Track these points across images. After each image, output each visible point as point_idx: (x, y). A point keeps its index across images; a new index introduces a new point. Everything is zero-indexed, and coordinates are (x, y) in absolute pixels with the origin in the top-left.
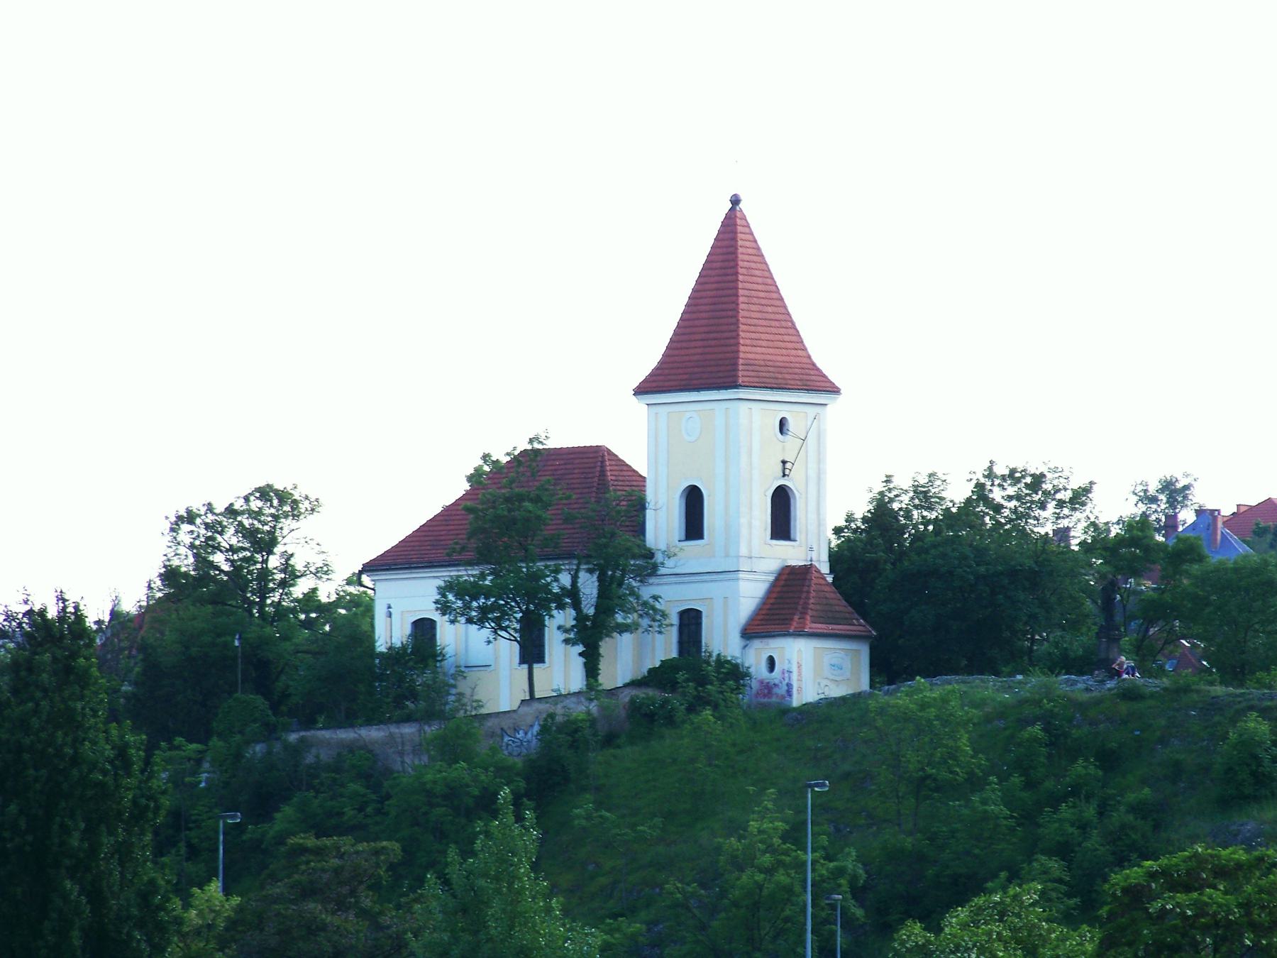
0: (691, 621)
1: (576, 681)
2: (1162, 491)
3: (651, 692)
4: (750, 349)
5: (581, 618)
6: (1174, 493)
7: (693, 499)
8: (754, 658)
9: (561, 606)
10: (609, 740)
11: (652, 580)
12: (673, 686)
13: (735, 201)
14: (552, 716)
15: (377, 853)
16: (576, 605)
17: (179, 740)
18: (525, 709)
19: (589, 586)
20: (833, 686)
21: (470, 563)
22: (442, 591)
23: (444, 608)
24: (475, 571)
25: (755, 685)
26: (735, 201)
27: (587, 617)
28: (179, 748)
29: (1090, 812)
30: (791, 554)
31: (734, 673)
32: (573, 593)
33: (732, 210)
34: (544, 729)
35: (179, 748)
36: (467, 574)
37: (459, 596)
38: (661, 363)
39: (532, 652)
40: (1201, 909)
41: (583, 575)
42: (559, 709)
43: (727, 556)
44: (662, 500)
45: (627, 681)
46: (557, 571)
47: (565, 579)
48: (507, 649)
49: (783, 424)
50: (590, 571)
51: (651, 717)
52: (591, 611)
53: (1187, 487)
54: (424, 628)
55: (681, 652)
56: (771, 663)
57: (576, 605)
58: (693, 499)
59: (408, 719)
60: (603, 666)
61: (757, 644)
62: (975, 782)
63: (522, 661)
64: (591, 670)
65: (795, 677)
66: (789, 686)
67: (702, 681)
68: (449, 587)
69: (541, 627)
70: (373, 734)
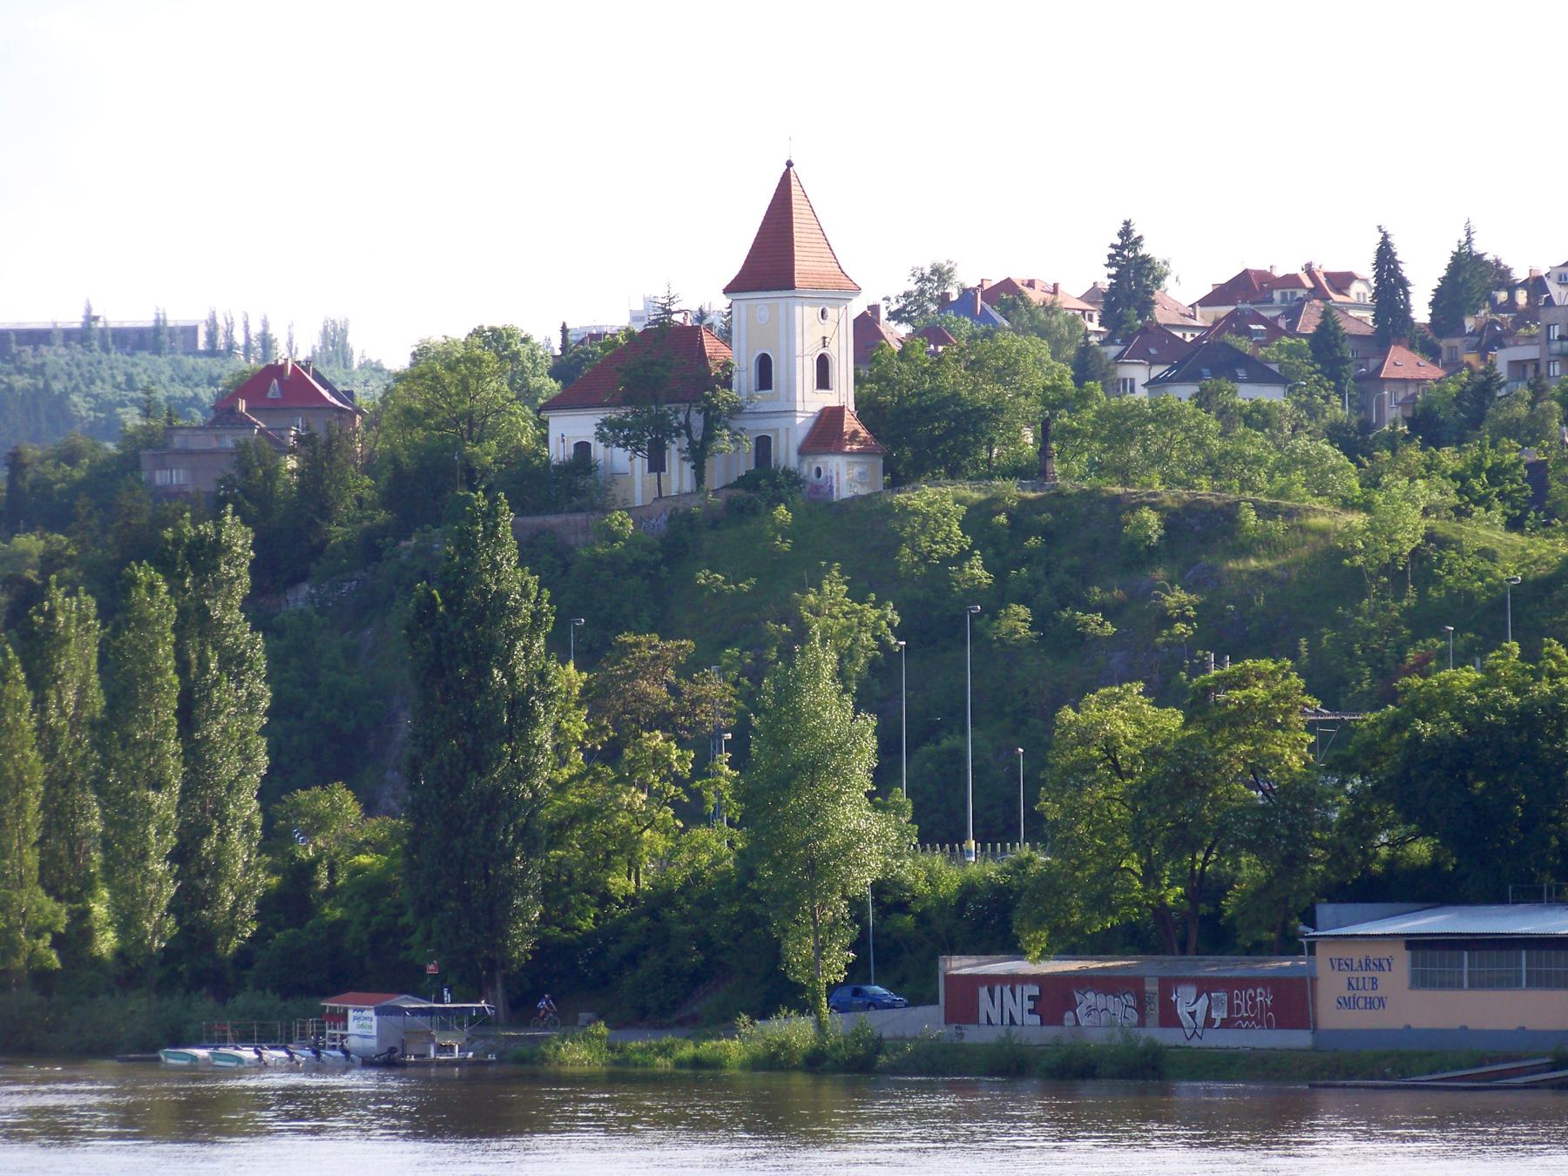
0: (763, 444)
1: (688, 485)
2: (933, 273)
3: (740, 492)
4: (805, 262)
5: (691, 443)
6: (941, 274)
7: (764, 363)
8: (807, 468)
9: (678, 436)
10: (714, 525)
11: (740, 416)
12: (757, 488)
13: (790, 164)
14: (676, 509)
15: (680, 647)
16: (689, 434)
17: (427, 526)
18: (656, 504)
19: (697, 421)
20: (859, 486)
21: (619, 406)
22: (600, 427)
23: (601, 437)
24: (622, 412)
25: (808, 487)
26: (790, 164)
27: (696, 443)
28: (428, 531)
29: (1040, 573)
30: (829, 399)
31: (793, 480)
32: (687, 427)
33: (788, 171)
34: (671, 518)
35: (428, 531)
36: (613, 414)
37: (611, 429)
38: (741, 272)
39: (657, 465)
40: (1250, 699)
41: (693, 414)
42: (680, 505)
43: (788, 400)
44: (744, 363)
45: (723, 484)
46: (677, 412)
47: (682, 417)
48: (641, 463)
49: (823, 312)
50: (699, 412)
51: (741, 509)
52: (699, 438)
53: (950, 270)
54: (583, 448)
55: (757, 465)
56: (819, 471)
57: (689, 434)
58: (764, 363)
59: (579, 510)
60: (707, 474)
61: (809, 459)
62: (965, 555)
63: (651, 470)
64: (699, 477)
65: (835, 480)
66: (831, 487)
67: (776, 486)
68: (605, 422)
69: (664, 447)
70: (553, 520)
